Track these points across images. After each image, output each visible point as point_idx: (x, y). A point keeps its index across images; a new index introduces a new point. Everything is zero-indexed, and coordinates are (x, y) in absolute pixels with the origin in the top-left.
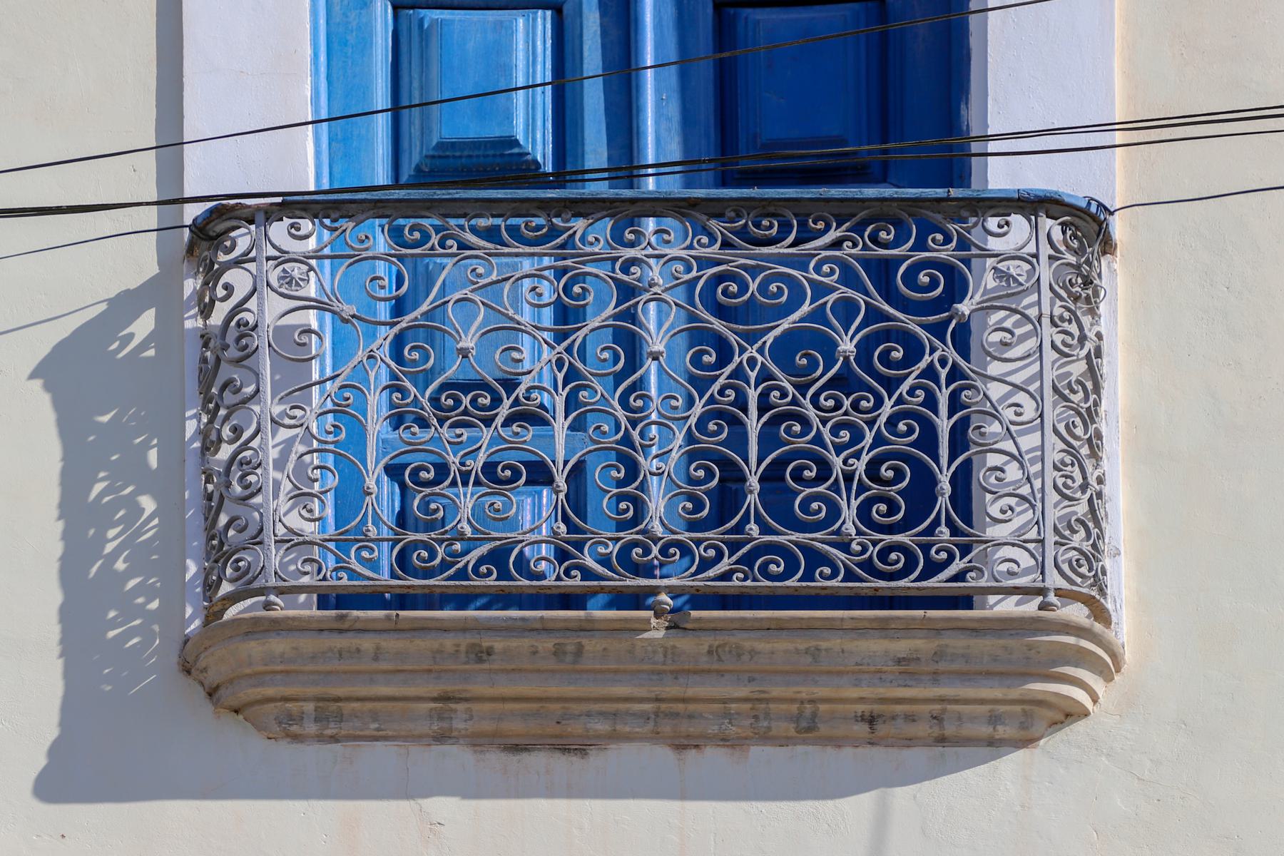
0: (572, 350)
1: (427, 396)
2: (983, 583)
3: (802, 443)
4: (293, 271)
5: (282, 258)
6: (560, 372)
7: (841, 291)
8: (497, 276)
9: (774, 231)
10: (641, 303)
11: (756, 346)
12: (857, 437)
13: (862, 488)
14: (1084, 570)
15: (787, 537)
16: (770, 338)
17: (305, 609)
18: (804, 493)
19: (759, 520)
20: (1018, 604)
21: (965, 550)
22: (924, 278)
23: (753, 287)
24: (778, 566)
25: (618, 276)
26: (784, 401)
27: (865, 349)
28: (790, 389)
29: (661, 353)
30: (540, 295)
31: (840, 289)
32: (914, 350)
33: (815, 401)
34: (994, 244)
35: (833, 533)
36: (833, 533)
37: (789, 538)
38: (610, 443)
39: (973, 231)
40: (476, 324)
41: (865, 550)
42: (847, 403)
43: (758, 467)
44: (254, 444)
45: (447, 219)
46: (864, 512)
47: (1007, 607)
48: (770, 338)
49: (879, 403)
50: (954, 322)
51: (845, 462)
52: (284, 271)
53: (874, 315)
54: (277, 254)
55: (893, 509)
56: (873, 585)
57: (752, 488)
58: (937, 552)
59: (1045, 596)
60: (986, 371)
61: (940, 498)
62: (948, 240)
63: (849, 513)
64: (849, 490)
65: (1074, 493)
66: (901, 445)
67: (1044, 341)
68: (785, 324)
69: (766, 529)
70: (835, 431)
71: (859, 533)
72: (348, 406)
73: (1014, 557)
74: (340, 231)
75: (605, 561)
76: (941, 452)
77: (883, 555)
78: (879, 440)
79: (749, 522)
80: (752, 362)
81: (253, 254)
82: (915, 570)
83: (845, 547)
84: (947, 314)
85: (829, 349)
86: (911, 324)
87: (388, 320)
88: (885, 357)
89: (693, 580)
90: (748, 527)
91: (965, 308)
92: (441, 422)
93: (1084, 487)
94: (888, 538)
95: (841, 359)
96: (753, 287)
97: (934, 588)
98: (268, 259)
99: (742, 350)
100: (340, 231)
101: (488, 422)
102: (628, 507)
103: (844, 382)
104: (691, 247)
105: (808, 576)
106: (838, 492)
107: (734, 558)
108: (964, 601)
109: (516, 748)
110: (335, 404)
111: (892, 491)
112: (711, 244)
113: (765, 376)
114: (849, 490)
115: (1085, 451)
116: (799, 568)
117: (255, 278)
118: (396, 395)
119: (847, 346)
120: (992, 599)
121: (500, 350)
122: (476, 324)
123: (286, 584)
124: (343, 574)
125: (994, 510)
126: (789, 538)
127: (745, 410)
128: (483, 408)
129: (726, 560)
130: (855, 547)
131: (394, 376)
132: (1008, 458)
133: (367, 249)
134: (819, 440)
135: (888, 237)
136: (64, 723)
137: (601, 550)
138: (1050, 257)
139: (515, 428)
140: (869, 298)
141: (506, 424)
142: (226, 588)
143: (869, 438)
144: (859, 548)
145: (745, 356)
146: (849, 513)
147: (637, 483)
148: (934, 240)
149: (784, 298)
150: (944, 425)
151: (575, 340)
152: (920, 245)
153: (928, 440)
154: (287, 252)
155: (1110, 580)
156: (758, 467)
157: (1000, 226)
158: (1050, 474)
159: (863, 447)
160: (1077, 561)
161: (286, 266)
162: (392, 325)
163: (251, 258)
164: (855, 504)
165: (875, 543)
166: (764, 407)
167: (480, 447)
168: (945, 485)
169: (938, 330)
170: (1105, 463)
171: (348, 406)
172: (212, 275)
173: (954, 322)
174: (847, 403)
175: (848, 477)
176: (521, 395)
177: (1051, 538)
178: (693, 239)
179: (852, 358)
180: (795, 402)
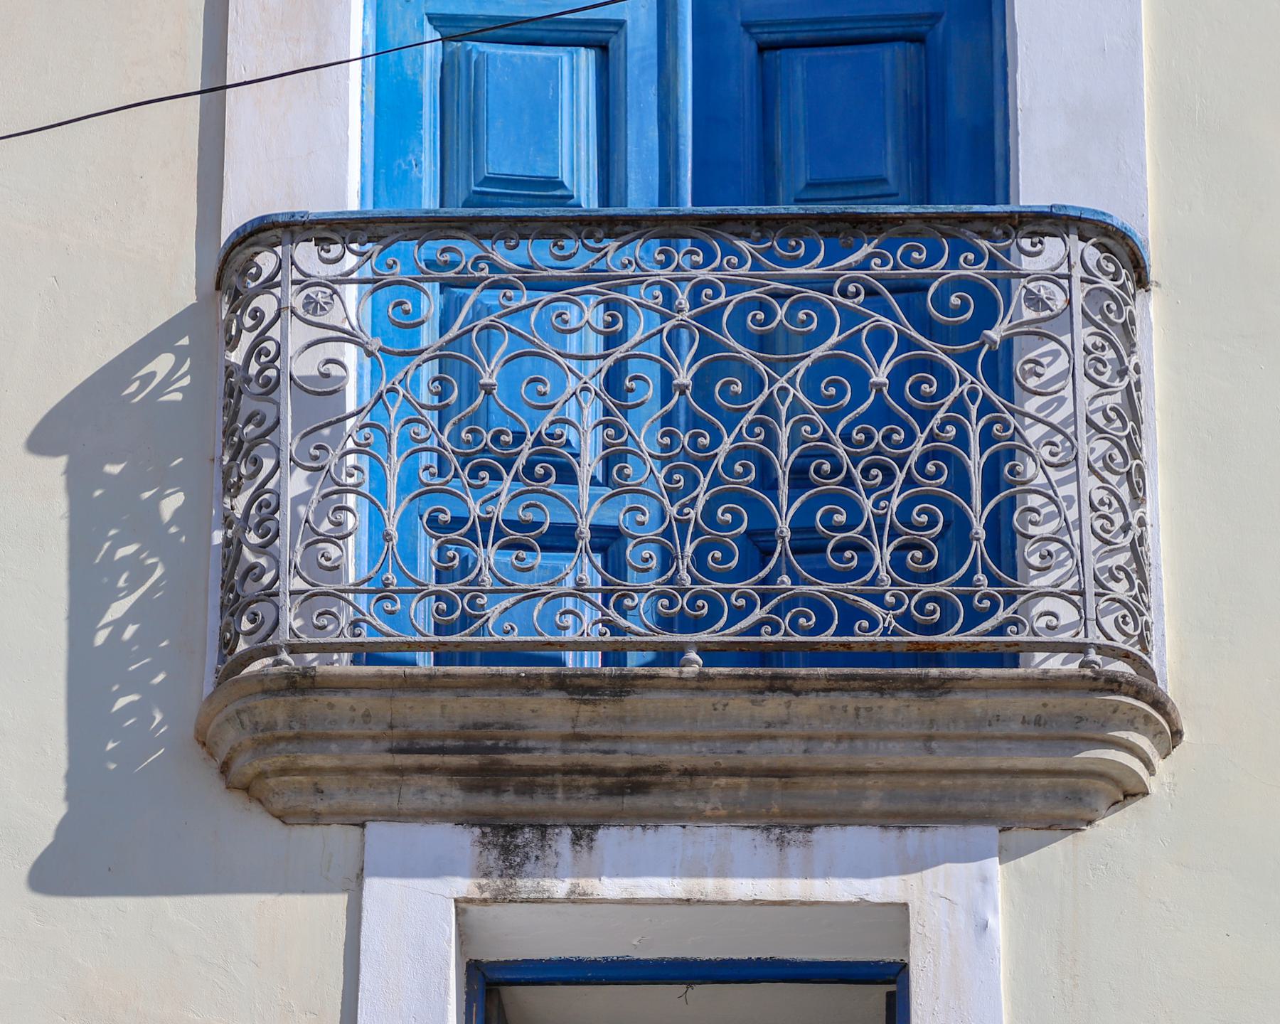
0: (795, 382)
1: (838, 432)
2: (1023, 637)
3: (832, 485)
4: (317, 296)
5: (305, 282)
6: (973, 404)
7: (873, 319)
8: (528, 300)
9: (802, 251)
10: (476, 329)
11: (785, 377)
12: (889, 476)
13: (894, 534)
14: (1130, 629)
15: (821, 588)
16: (803, 366)
17: (425, 663)
18: (837, 538)
19: (986, 571)
20: (1064, 663)
21: (1010, 598)
22: (954, 300)
23: (781, 313)
24: (809, 619)
25: (838, 299)
26: (816, 436)
27: (897, 377)
29: (687, 387)
30: (566, 322)
31: (874, 316)
32: (947, 383)
33: (846, 438)
34: (1027, 264)
35: (866, 584)
36: (866, 584)
37: (820, 589)
38: (832, 484)
40: (501, 350)
41: (900, 602)
42: (878, 437)
43: (983, 509)
44: (270, 485)
45: (482, 241)
46: (898, 563)
47: (1055, 664)
48: (803, 366)
49: (911, 438)
50: (986, 347)
51: (875, 505)
52: (308, 296)
53: (907, 343)
54: (301, 277)
55: (728, 556)
56: (909, 639)
57: (582, 536)
58: (980, 601)
59: (1086, 653)
60: (1023, 407)
61: (975, 543)
62: (978, 260)
63: (882, 557)
64: (880, 537)
65: (1116, 536)
66: (932, 486)
67: (1076, 366)
68: (818, 352)
69: (796, 580)
70: (865, 472)
71: (894, 583)
72: (368, 445)
73: (1051, 610)
74: (603, 253)
77: (920, 607)
78: (909, 482)
79: (976, 573)
80: (973, 393)
81: (278, 278)
82: (831, 625)
83: (878, 599)
84: (978, 342)
85: (861, 379)
86: (937, 351)
87: (603, 352)
88: (915, 389)
89: (723, 635)
90: (975, 578)
91: (996, 334)
93: (1126, 529)
94: (927, 588)
96: (781, 313)
97: (974, 643)
98: (294, 283)
99: (773, 381)
100: (603, 253)
102: (853, 557)
103: (880, 414)
104: (720, 268)
105: (845, 629)
106: (870, 538)
107: (767, 607)
108: (1009, 657)
109: (860, 825)
110: (356, 443)
111: (926, 537)
112: (740, 265)
113: (796, 407)
114: (880, 537)
115: (1124, 492)
116: (833, 620)
117: (279, 301)
118: (611, 431)
119: (880, 375)
120: (1039, 656)
121: (526, 381)
122: (501, 350)
123: (1039, 639)
125: (1035, 560)
126: (820, 589)
127: (966, 448)
129: (757, 610)
130: (889, 599)
131: (607, 412)
132: (1046, 500)
133: (393, 274)
134: (849, 481)
135: (920, 257)
136: (71, 796)
138: (1083, 280)
140: (898, 325)
142: (242, 646)
143: (901, 476)
144: (893, 600)
145: (776, 387)
147: (860, 528)
148: (965, 260)
149: (814, 326)
150: (975, 462)
151: (798, 371)
152: (953, 264)
153: (961, 482)
154: (309, 276)
155: (1154, 636)
156: (983, 509)
157: (1033, 245)
158: (1088, 514)
159: (893, 490)
160: (1124, 617)
161: (309, 291)
162: (605, 357)
163: (351, 279)
164: (888, 552)
165: (911, 594)
167: (893, 490)
168: (979, 529)
169: (967, 361)
170: (1148, 507)
171: (368, 445)
172: (239, 299)
173: (986, 347)
174: (878, 437)
176: (543, 432)
177: (1091, 589)
178: (722, 261)
179: (885, 390)
180: (825, 438)
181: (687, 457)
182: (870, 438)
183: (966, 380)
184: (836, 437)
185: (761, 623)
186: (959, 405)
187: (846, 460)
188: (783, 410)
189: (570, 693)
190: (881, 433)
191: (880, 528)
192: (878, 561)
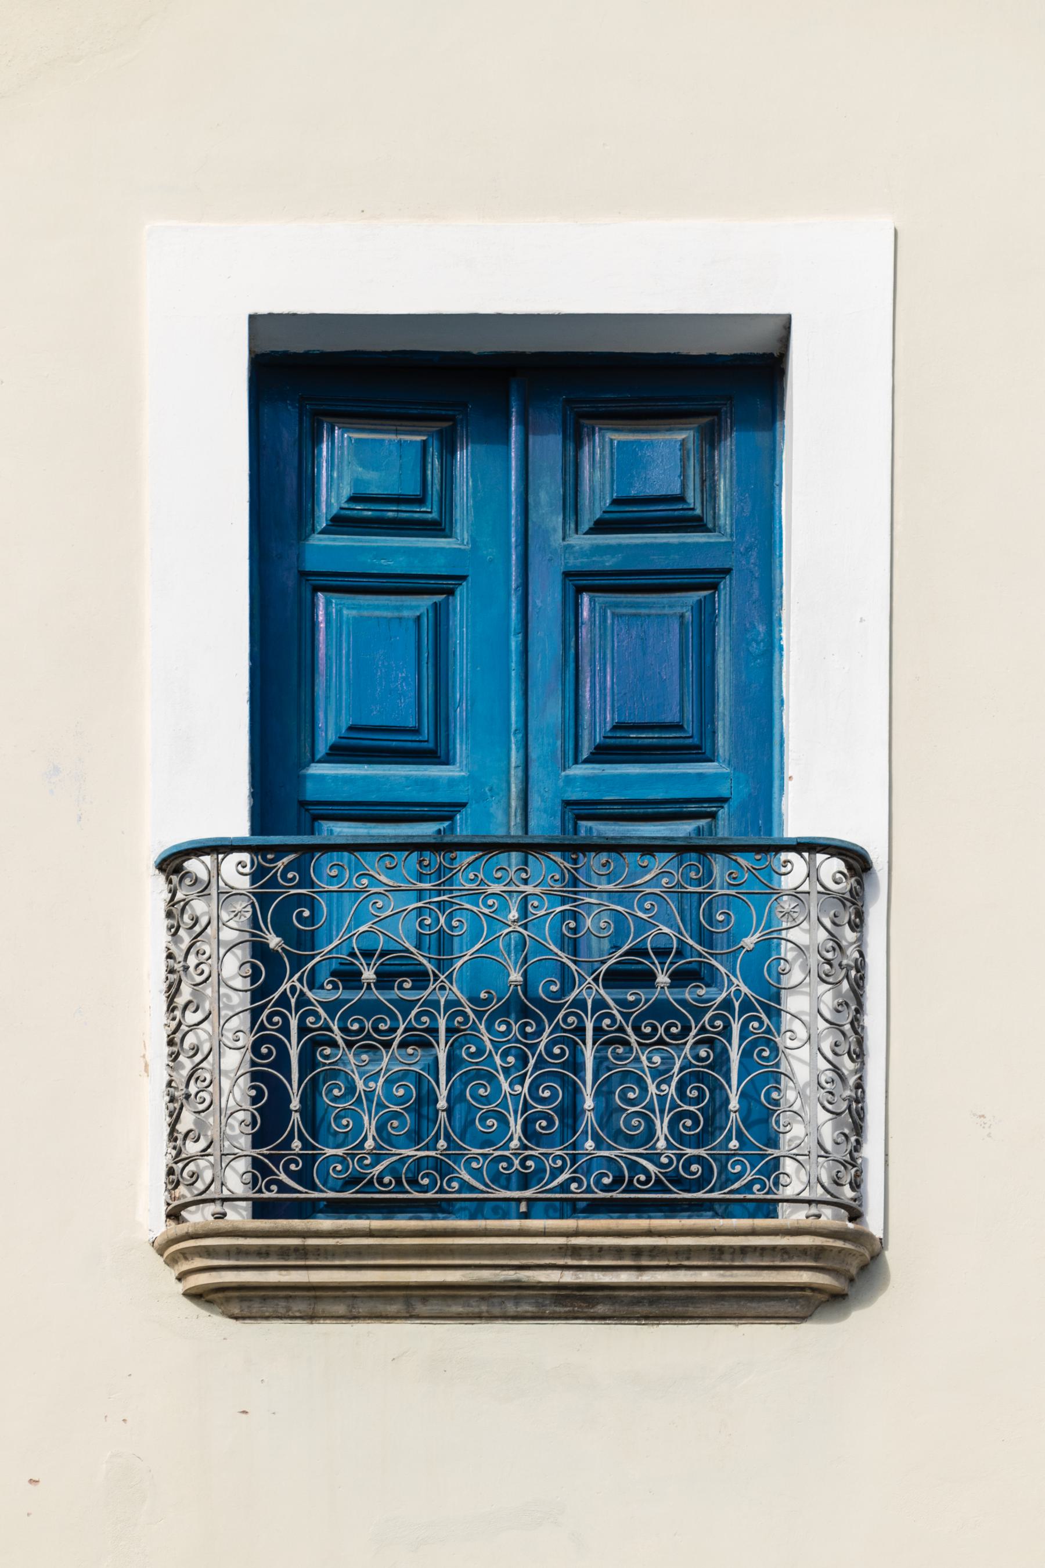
15: (617, 1152)
19: (301, 1137)
28: (619, 1017)
39: (581, 870)
63: (662, 1128)
69: (599, 1144)
75: (476, 1173)
76: (293, 1076)
92: (350, 1045)
95: (365, 984)
101: (387, 1045)
124: (274, 1187)
128: (673, 1037)
137: (474, 1165)
139: (410, 1050)
141: (403, 1045)
145: (733, 989)
146: (662, 1128)
166: (303, 1030)
174: (661, 1030)
175: (662, 1099)
180: (621, 1029)
181: (518, 1041)
182: (655, 1029)
183: (733, 984)
184: (629, 1030)
185: (751, 1183)
186: (283, 1001)
187: (489, 1046)
188: (293, 1001)
189: (454, 1214)
190: (371, 1022)
191: (370, 1100)
192: (512, 1128)
